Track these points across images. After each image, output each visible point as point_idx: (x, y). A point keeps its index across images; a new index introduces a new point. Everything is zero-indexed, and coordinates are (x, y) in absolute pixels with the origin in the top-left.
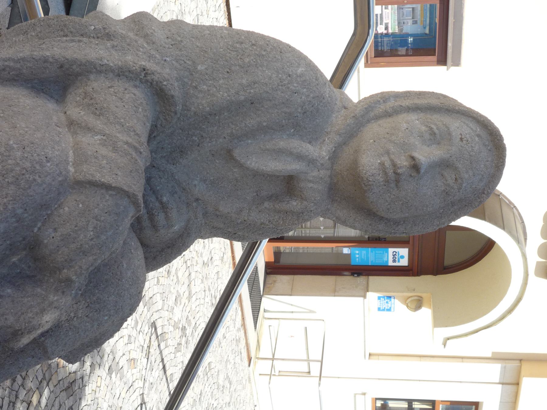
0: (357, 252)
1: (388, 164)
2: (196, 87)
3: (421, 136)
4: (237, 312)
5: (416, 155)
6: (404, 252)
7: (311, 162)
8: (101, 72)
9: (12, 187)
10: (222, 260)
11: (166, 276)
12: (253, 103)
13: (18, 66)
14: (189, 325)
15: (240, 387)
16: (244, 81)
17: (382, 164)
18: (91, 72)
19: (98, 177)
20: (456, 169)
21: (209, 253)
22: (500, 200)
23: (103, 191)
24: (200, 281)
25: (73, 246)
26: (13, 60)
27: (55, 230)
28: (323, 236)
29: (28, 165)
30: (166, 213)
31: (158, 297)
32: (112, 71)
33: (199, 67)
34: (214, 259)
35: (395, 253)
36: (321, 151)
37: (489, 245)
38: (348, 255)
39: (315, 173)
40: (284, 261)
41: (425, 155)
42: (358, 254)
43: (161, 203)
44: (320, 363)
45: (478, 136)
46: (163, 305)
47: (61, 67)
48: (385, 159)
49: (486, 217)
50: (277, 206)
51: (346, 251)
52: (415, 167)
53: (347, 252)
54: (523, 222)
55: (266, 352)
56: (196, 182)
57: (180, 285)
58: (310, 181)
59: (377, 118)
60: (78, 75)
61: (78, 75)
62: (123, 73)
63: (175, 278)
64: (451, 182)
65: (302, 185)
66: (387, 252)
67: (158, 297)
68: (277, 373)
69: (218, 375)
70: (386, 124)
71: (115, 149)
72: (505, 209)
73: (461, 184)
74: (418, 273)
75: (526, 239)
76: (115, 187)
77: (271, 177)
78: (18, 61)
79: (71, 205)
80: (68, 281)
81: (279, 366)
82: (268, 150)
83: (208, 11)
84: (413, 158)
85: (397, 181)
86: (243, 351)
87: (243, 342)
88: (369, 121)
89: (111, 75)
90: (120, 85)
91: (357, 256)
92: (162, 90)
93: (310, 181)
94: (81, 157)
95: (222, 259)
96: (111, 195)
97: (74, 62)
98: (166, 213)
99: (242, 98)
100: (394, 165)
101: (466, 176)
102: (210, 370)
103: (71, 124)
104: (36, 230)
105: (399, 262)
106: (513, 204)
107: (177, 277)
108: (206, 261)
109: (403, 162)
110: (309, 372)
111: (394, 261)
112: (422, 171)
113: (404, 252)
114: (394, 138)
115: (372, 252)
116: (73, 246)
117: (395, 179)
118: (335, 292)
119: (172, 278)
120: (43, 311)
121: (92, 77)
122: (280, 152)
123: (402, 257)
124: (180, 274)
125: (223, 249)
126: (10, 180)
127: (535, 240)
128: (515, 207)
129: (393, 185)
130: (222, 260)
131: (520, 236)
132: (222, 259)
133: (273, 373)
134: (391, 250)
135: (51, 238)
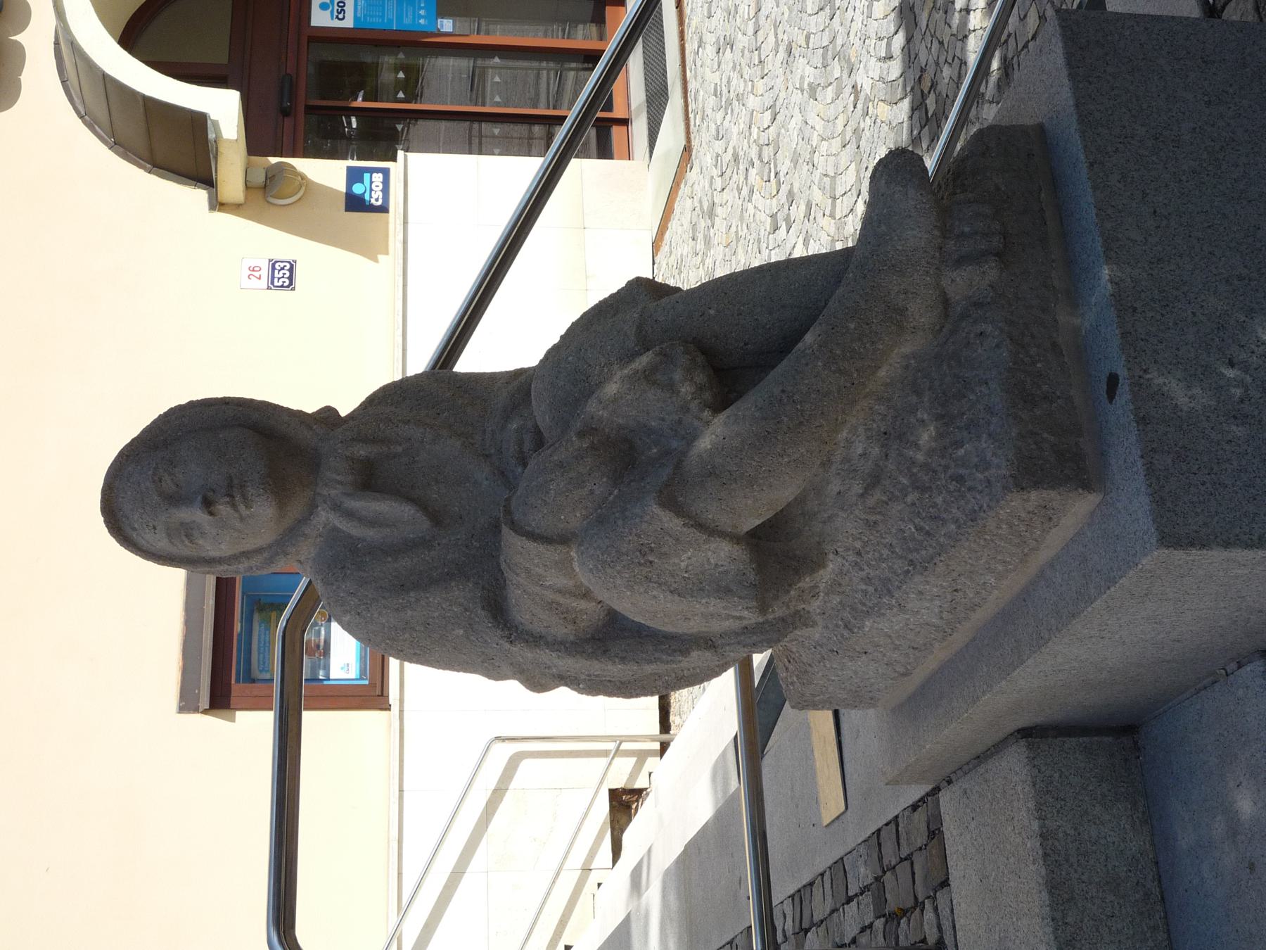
0: (422, 21)
1: (242, 508)
2: (466, 610)
3: (203, 534)
5: (207, 517)
7: (337, 507)
8: (561, 643)
9: (624, 550)
10: (701, 39)
11: (794, 45)
12: (402, 586)
13: (657, 655)
16: (409, 613)
17: (248, 507)
18: (572, 643)
19: (541, 548)
20: (160, 495)
21: (723, 66)
22: (113, 134)
23: (537, 531)
24: (740, 10)
25: (573, 474)
26: (662, 662)
27: (592, 492)
28: (497, 60)
29: (609, 571)
30: (521, 452)
32: (547, 644)
33: (461, 632)
34: (715, 49)
35: (341, 16)
36: (324, 516)
37: (130, 39)
38: (442, 14)
39: (333, 492)
41: (196, 515)
42: (420, 17)
45: (134, 529)
47: (605, 652)
49: (141, 103)
50: (385, 449)
51: (447, 25)
52: (208, 504)
53: (445, 21)
54: (63, 82)
56: (486, 483)
57: (773, 16)
58: (341, 483)
59: (259, 551)
60: (587, 641)
61: (587, 641)
63: (780, 36)
64: (166, 477)
65: (350, 478)
66: (356, 19)
70: (250, 544)
71: (528, 571)
72: (101, 113)
73: (154, 474)
75: (57, 43)
76: (522, 535)
78: (657, 660)
79: (574, 519)
80: (581, 434)
82: (388, 526)
84: (211, 514)
85: (230, 486)
88: (270, 546)
89: (550, 639)
90: (537, 628)
91: (422, 12)
92: (494, 617)
93: (341, 483)
94: (565, 566)
96: (529, 525)
97: (589, 657)
98: (521, 452)
99: (412, 594)
100: (234, 506)
101: (148, 484)
103: (587, 595)
104: (616, 492)
106: (85, 122)
108: (729, 50)
109: (223, 509)
112: (200, 498)
114: (236, 534)
115: (391, 21)
116: (573, 474)
117: (233, 490)
119: (786, 38)
120: (615, 400)
121: (572, 638)
122: (373, 522)
124: (771, 39)
125: (699, 63)
126: (625, 558)
127: (36, 40)
128: (81, 117)
129: (236, 481)
130: (701, 39)
131: (68, 52)
132: (701, 43)
134: (348, 23)
135: (599, 486)
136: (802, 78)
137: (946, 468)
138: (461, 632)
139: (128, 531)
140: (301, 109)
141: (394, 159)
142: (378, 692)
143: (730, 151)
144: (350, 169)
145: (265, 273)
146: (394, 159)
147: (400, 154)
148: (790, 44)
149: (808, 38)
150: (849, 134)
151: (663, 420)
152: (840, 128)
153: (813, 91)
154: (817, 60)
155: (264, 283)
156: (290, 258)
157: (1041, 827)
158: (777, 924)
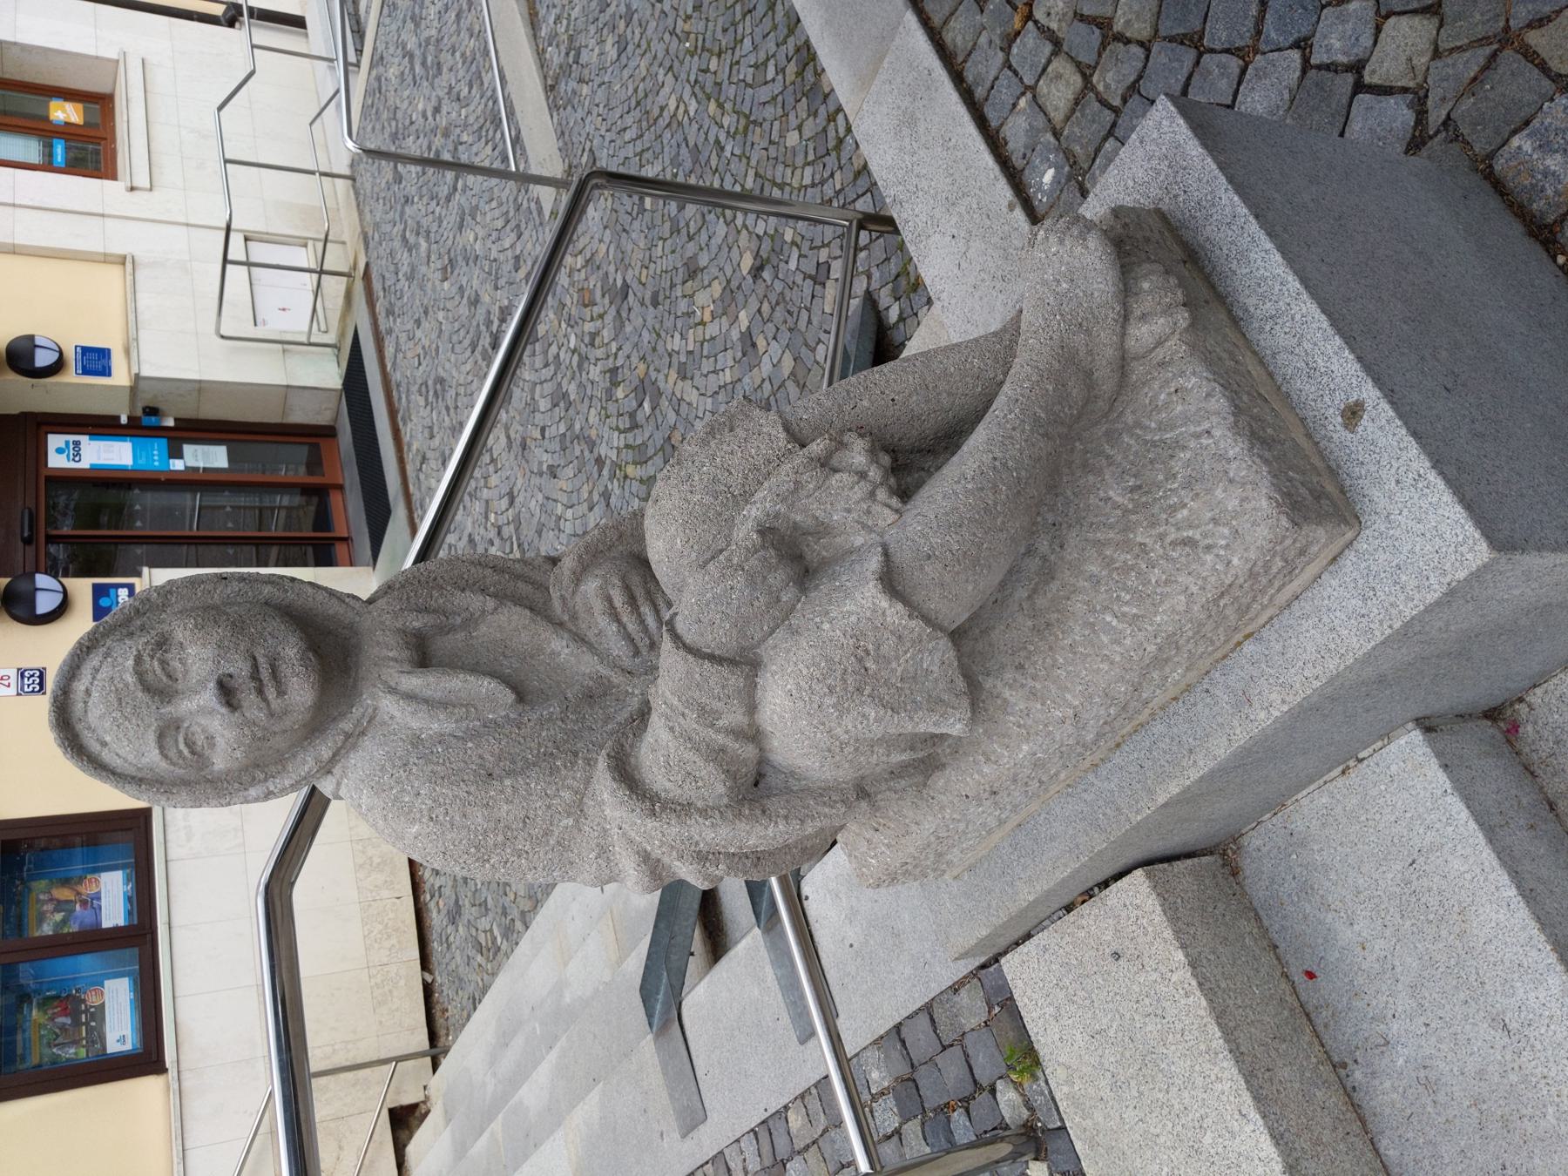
4: (394, 364)
6: (57, 461)
14: (485, 350)
15: (387, 228)
31: (544, 404)
40: (302, 452)
43: (619, 621)
44: (230, 257)
45: (104, 744)
46: (533, 391)
48: (276, 704)
55: (335, 288)
58: (396, 660)
62: (683, 809)
67: (544, 404)
68: (310, 243)
69: (429, 257)
74: (26, 417)
77: (454, 664)
81: (304, 258)
83: (455, 887)
86: (381, 294)
87: (380, 307)
92: (631, 789)
95: (424, 459)
102: (444, 269)
105: (67, 443)
107: (508, 437)
110: (246, 239)
111: (77, 444)
113: (57, 461)
118: (200, 388)
123: (59, 451)
125: (422, 476)
133: (320, 245)
136: (540, 463)
137: (1162, 537)
138: (570, 822)
139: (94, 747)
140: (42, 539)
141: (139, 575)
142: (154, 1058)
143: (465, 539)
144: (95, 586)
145: (13, 681)
146: (139, 575)
147: (145, 570)
148: (524, 440)
149: (543, 430)
150: (596, 497)
151: (849, 511)
152: (586, 496)
153: (553, 472)
154: (556, 446)
155: (13, 690)
156: (40, 666)
157: (1187, 956)
158: (732, 1165)
